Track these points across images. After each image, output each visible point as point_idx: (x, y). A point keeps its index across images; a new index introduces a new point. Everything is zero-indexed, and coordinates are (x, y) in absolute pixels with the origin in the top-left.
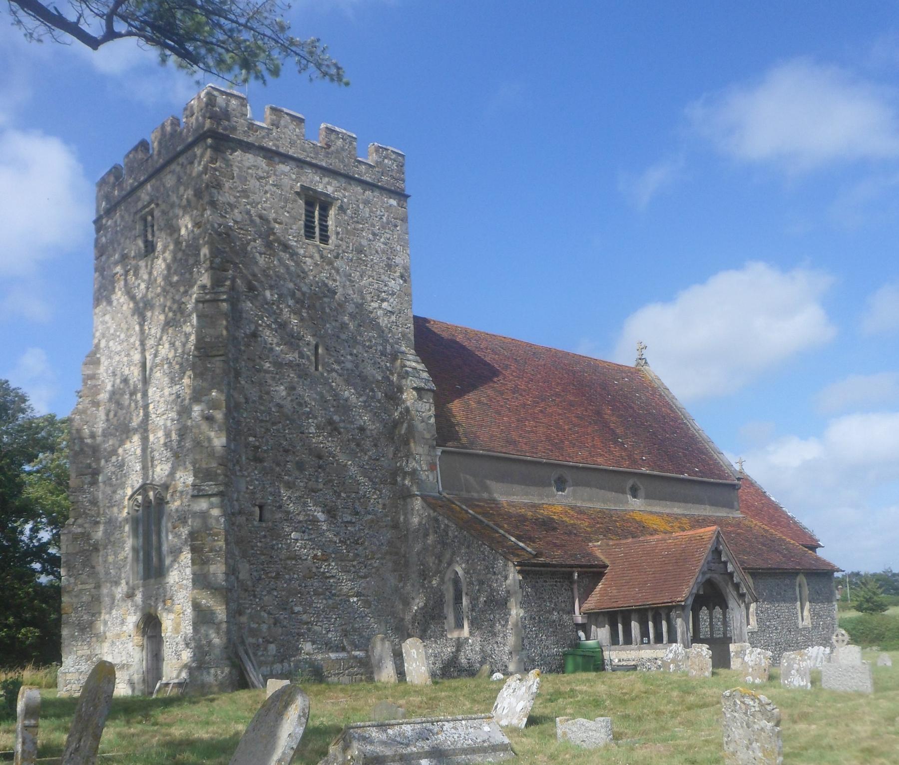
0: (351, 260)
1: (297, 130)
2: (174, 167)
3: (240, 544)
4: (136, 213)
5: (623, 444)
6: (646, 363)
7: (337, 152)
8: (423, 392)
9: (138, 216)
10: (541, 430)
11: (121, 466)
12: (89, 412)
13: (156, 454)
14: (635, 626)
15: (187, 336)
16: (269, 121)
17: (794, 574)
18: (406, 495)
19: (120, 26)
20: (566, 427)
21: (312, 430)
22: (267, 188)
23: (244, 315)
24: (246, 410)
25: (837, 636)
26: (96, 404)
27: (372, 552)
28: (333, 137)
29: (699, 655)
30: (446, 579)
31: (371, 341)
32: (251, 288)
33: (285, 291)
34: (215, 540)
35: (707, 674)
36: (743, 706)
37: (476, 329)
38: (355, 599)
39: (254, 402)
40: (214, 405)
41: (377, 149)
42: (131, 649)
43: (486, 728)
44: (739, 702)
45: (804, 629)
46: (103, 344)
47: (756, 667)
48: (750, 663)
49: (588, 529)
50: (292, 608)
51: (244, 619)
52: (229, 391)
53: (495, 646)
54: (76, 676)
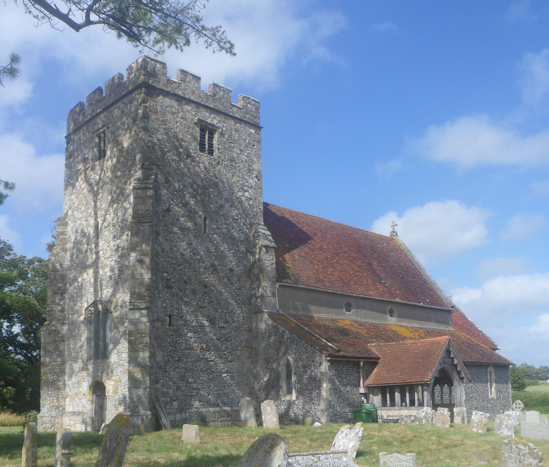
0: (227, 166)
1: (196, 84)
2: (120, 104)
3: (157, 340)
4: (93, 133)
5: (384, 283)
6: (397, 234)
7: (220, 99)
8: (269, 249)
9: (95, 134)
11: (80, 288)
12: (60, 255)
13: (104, 282)
14: (397, 395)
15: (126, 209)
16: (179, 78)
17: (487, 366)
18: (258, 311)
19: (93, 17)
20: (351, 272)
21: (202, 270)
22: (177, 120)
23: (162, 198)
24: (162, 256)
25: (516, 404)
26: (65, 250)
27: (236, 346)
28: (217, 89)
29: (442, 414)
30: (282, 363)
31: (238, 216)
32: (168, 181)
33: (187, 184)
34: (143, 337)
36: (517, 450)
37: (297, 211)
38: (225, 375)
39: (167, 252)
40: (144, 254)
41: (244, 98)
42: (85, 403)
44: (514, 447)
45: (493, 399)
46: (70, 213)
48: (476, 421)
49: (366, 335)
50: (187, 380)
51: (159, 386)
52: (153, 245)
53: (312, 405)
54: (49, 419)
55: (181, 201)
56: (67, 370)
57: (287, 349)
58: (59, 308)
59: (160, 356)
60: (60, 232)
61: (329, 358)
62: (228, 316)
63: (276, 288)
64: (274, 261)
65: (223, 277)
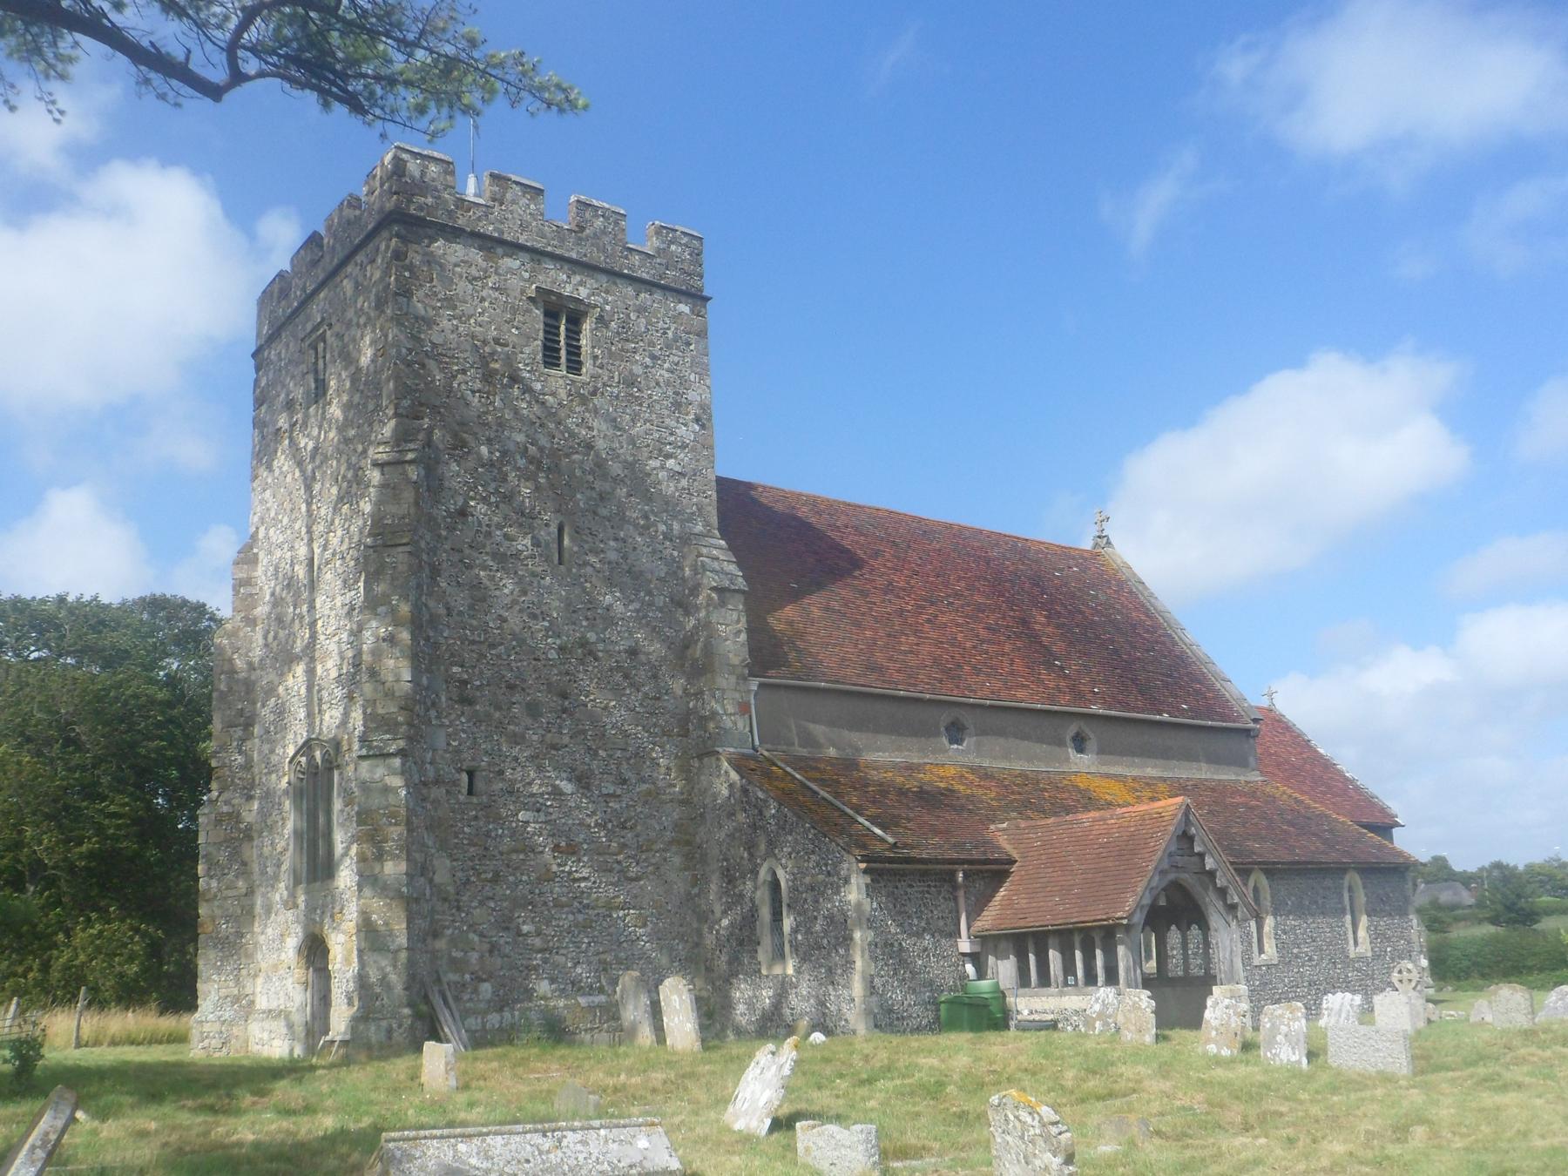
0: (617, 397)
5: (1062, 668)
6: (1109, 543)
10: (925, 649)
11: (281, 712)
13: (325, 694)
14: (1054, 957)
16: (488, 194)
18: (707, 752)
20: (968, 645)
21: (553, 655)
22: (484, 293)
23: (446, 484)
25: (1400, 972)
33: (512, 447)
35: (1149, 1038)
38: (621, 913)
39: (460, 613)
41: (659, 231)
43: (642, 1143)
45: (1360, 959)
46: (261, 534)
47: (1222, 1029)
48: (1214, 1023)
51: (441, 944)
55: (496, 489)
56: (258, 909)
57: (771, 844)
58: (240, 759)
59: (443, 869)
60: (240, 580)
61: (863, 866)
62: (625, 766)
63: (749, 691)
64: (743, 625)
65: (611, 670)
